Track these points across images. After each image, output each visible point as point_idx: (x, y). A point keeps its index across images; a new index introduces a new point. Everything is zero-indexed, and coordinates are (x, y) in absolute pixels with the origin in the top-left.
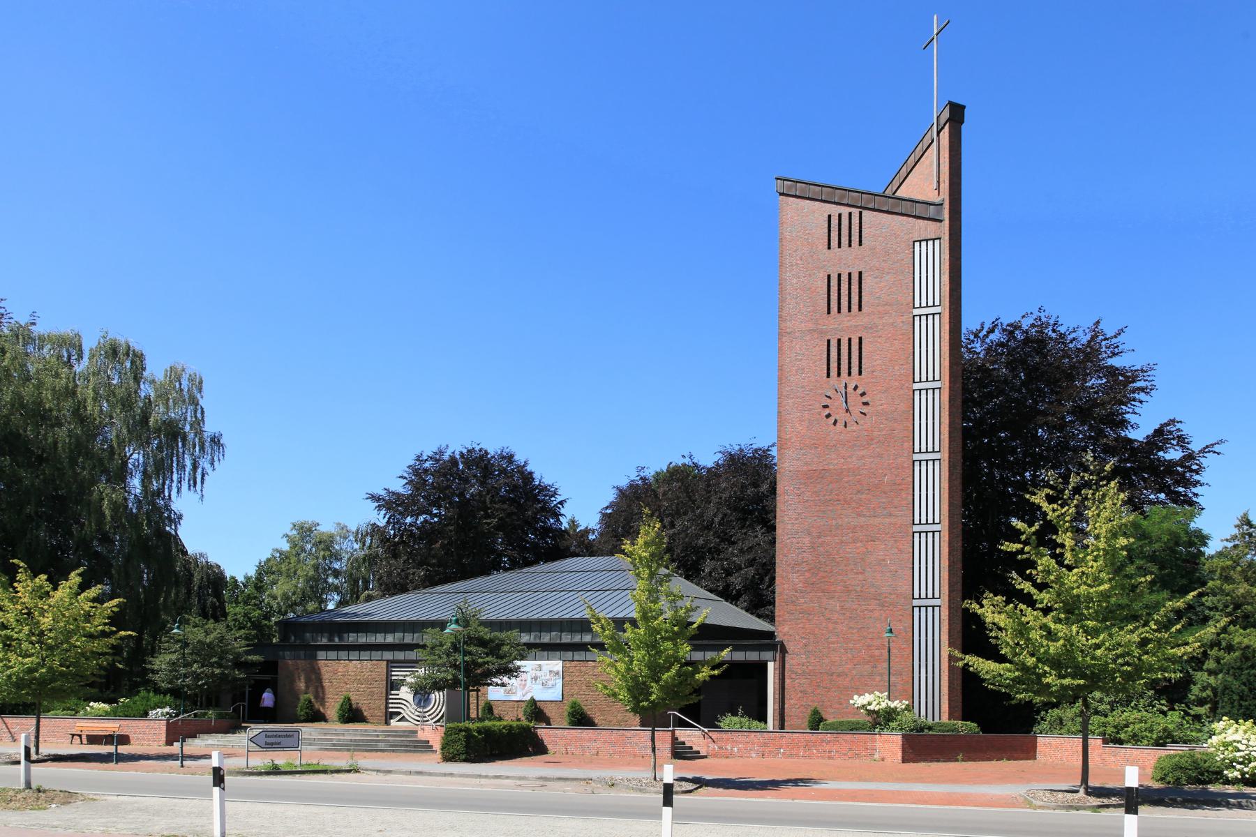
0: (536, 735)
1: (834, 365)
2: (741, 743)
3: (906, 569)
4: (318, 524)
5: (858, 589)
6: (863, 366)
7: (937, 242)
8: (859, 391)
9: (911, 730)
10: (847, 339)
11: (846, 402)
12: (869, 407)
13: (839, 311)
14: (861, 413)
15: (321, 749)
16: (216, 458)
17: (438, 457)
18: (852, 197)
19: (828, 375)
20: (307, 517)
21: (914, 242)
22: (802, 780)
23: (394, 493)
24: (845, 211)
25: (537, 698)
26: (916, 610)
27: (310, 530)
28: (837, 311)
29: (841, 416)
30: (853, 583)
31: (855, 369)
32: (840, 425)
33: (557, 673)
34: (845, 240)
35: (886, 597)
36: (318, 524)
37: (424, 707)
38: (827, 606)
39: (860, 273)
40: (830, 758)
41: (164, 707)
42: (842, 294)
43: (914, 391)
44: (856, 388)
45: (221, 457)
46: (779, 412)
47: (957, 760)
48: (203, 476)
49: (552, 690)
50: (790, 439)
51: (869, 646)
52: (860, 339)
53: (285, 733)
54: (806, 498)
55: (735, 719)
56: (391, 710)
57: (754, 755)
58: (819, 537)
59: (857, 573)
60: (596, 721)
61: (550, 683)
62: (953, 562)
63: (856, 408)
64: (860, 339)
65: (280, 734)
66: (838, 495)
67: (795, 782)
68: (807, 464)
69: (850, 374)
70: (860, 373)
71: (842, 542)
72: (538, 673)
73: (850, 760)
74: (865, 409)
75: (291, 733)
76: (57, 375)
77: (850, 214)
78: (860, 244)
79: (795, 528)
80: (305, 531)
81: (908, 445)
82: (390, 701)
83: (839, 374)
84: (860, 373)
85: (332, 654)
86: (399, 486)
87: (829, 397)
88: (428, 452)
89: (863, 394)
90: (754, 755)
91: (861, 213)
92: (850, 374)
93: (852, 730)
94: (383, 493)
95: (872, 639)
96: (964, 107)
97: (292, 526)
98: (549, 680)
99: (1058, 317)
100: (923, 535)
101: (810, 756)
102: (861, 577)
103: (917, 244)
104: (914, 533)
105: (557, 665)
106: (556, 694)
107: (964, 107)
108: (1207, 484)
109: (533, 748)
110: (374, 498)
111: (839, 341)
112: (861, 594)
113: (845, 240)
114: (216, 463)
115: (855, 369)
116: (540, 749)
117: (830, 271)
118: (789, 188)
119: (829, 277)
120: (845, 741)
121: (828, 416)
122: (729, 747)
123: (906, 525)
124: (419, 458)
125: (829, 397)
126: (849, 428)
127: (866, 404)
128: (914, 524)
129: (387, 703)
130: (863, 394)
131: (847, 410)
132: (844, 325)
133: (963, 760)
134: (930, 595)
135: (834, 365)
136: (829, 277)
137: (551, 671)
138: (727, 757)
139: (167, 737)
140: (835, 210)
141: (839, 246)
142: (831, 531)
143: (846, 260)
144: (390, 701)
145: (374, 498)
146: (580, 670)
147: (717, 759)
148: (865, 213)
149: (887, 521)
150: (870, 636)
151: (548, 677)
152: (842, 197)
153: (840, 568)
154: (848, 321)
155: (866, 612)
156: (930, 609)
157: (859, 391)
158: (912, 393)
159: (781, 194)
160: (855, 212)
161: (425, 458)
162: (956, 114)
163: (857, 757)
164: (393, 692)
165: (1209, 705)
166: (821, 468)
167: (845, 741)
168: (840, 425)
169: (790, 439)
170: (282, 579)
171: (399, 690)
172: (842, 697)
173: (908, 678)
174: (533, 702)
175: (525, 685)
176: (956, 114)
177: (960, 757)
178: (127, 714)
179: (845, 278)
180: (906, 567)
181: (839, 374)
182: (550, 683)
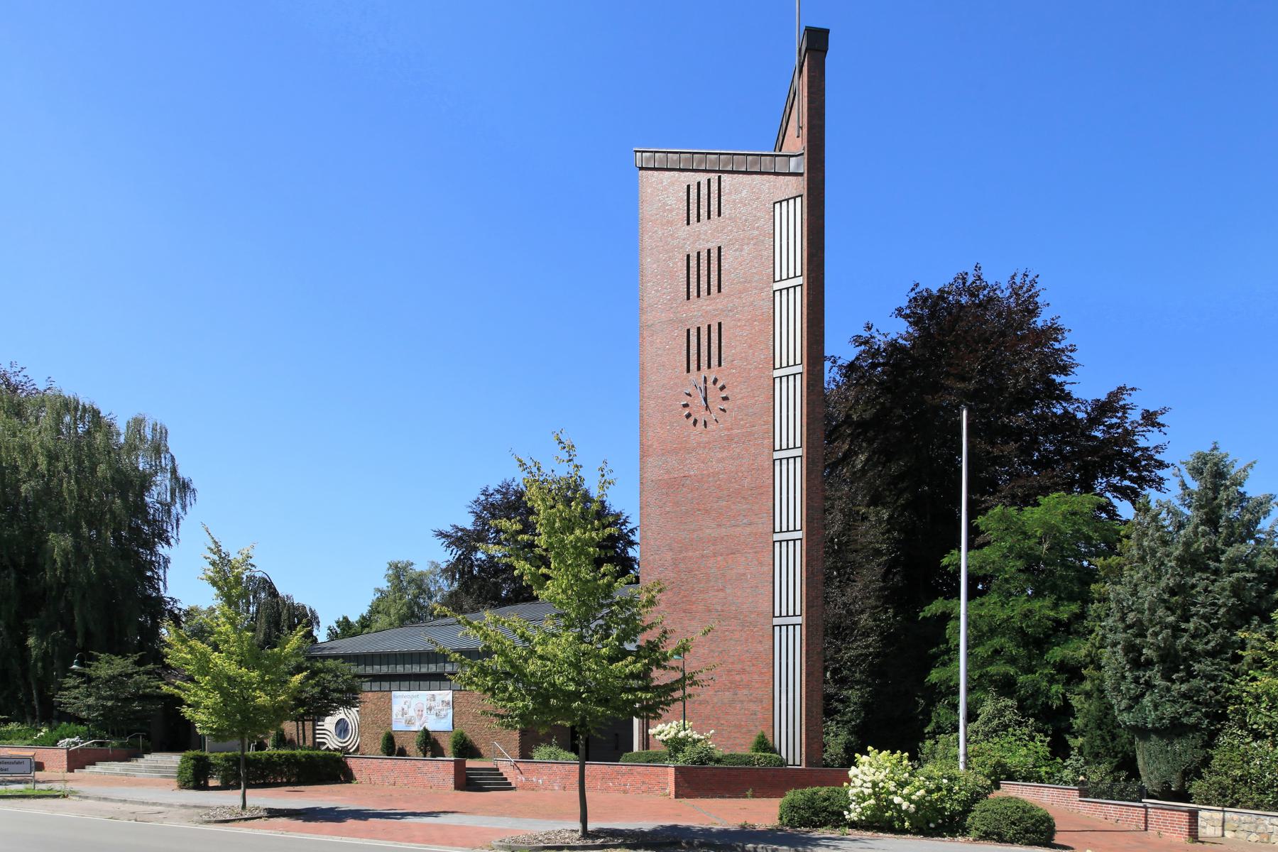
0: (346, 764)
1: (694, 357)
2: (545, 775)
3: (766, 584)
4: (412, 564)
5: (719, 608)
6: (723, 356)
7: (799, 200)
8: (719, 385)
9: (694, 763)
10: (706, 326)
11: (705, 399)
12: (729, 402)
13: (699, 296)
14: (721, 409)
15: (162, 777)
16: (188, 502)
17: (504, 490)
18: (710, 161)
19: (688, 371)
20: (401, 557)
21: (774, 204)
22: (434, 813)
23: (462, 530)
24: (703, 178)
25: (430, 728)
26: (777, 629)
27: (405, 569)
28: (696, 294)
29: (701, 415)
30: (714, 602)
31: (714, 361)
32: (700, 425)
33: (448, 703)
34: (704, 211)
35: (746, 616)
36: (412, 564)
37: (344, 738)
38: (689, 629)
39: (719, 248)
40: (625, 792)
41: (74, 737)
42: (701, 275)
43: (774, 379)
44: (715, 381)
45: (193, 502)
46: (641, 416)
47: (745, 797)
48: (178, 520)
49: (443, 721)
50: (651, 445)
51: (729, 671)
52: (720, 324)
53: (13, 760)
54: (667, 509)
55: (549, 749)
56: (318, 740)
57: (556, 788)
58: (681, 552)
59: (718, 591)
60: (482, 752)
61: (443, 713)
62: (812, 573)
63: (716, 404)
64: (720, 324)
65: (5, 760)
66: (698, 504)
67: (453, 812)
68: (668, 472)
69: (709, 366)
70: (720, 364)
71: (703, 556)
72: (433, 704)
73: (644, 795)
74: (725, 405)
75: (21, 760)
76: (14, 435)
77: (709, 181)
78: (719, 215)
79: (657, 543)
80: (399, 572)
81: (768, 442)
82: (318, 732)
83: (699, 368)
84: (720, 364)
85: (376, 686)
86: (468, 522)
87: (689, 395)
88: (493, 486)
89: (723, 388)
90: (556, 788)
91: (720, 177)
92: (709, 366)
93: (649, 762)
94: (449, 530)
95: (733, 663)
96: (827, 32)
97: (388, 566)
98: (441, 710)
99: (1038, 276)
100: (784, 544)
101: (607, 789)
102: (721, 594)
103: (777, 206)
104: (774, 542)
105: (447, 695)
106: (447, 724)
107: (827, 32)
108: (1172, 465)
109: (344, 777)
110: (441, 534)
111: (699, 329)
112: (722, 613)
113: (704, 211)
114: (188, 509)
115: (714, 361)
116: (348, 777)
117: (688, 249)
118: (648, 159)
119: (688, 256)
120: (639, 773)
121: (688, 416)
122: (534, 780)
123: (766, 534)
124: (484, 492)
125: (689, 395)
126: (710, 427)
127: (725, 399)
128: (774, 532)
129: (314, 734)
130: (723, 388)
131: (707, 407)
132: (702, 311)
133: (753, 796)
134: (791, 613)
135: (694, 357)
136: (688, 256)
137: (443, 701)
138: (533, 790)
139: (68, 764)
140: (692, 178)
141: (699, 220)
142: (692, 545)
143: (705, 235)
144: (318, 732)
145: (441, 534)
146: (467, 699)
147: (524, 791)
148: (724, 177)
149: (748, 530)
150: (730, 660)
151: (441, 707)
152: (700, 162)
153: (702, 585)
154: (707, 305)
155: (727, 633)
156: (791, 628)
157: (719, 385)
158: (772, 381)
159: (642, 168)
160: (714, 177)
161: (491, 492)
162: (817, 41)
163: (649, 791)
164: (319, 723)
165: (1137, 739)
166: (682, 475)
167: (639, 773)
168: (700, 425)
169: (651, 445)
170: (1210, 636)
171: (323, 721)
172: (704, 726)
173: (767, 702)
174: (426, 733)
175: (422, 715)
176: (817, 41)
177: (749, 793)
178: (43, 743)
179: (704, 255)
180: (767, 581)
181: (699, 368)
182: (443, 713)
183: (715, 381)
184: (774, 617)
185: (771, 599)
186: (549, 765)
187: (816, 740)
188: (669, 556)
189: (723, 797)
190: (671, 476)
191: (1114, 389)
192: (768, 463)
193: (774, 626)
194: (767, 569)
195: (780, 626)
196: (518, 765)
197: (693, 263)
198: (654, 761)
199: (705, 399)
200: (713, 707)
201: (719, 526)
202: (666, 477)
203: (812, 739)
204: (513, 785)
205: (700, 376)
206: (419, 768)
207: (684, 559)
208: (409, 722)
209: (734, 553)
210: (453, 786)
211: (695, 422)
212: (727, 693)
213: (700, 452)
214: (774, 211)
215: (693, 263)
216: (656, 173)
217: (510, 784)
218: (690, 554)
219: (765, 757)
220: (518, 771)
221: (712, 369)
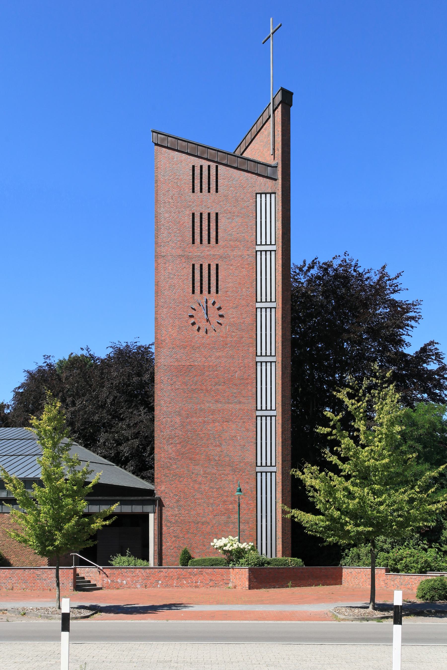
1: (197, 284)
5: (217, 458)
8: (217, 306)
11: (207, 314)
19: (193, 292)
21: (256, 194)
24: (205, 164)
29: (203, 325)
31: (213, 289)
32: (202, 332)
35: (237, 465)
40: (196, 587)
44: (214, 303)
46: (156, 319)
47: (287, 587)
51: (224, 502)
52: (217, 265)
55: (124, 558)
57: (139, 586)
58: (187, 417)
59: (216, 446)
60: (12, 562)
62: (285, 439)
63: (214, 319)
64: (217, 265)
67: (169, 607)
68: (177, 360)
69: (209, 292)
71: (204, 422)
73: (211, 588)
74: (221, 320)
81: (252, 349)
83: (201, 292)
89: (219, 309)
90: (139, 586)
92: (209, 292)
93: (212, 565)
101: (182, 586)
102: (218, 449)
104: (257, 416)
113: (205, 186)
115: (213, 289)
117: (194, 209)
120: (208, 574)
122: (119, 581)
123: (251, 410)
130: (219, 309)
133: (292, 586)
135: (197, 284)
140: (198, 162)
141: (201, 192)
149: (238, 407)
152: (203, 152)
153: (203, 442)
157: (217, 306)
158: (255, 310)
159: (157, 144)
160: (213, 165)
166: (188, 364)
167: (208, 574)
168: (202, 332)
177: (290, 584)
179: (205, 216)
180: (252, 442)
183: (214, 303)
184: (257, 466)
185: (255, 454)
186: (132, 570)
187: (287, 548)
188: (178, 420)
189: (310, 585)
190: (180, 363)
191: (422, 346)
192: (252, 364)
193: (257, 472)
194: (253, 434)
195: (261, 472)
196: (105, 570)
197: (197, 220)
198: (216, 565)
199: (207, 314)
200: (213, 527)
201: (217, 401)
202: (176, 364)
203: (285, 548)
204: (98, 586)
205: (202, 298)
206: (38, 575)
207: (190, 423)
208: (164, 537)
209: (228, 422)
210: (72, 588)
211: (199, 329)
212: (223, 517)
213: (203, 350)
214: (256, 198)
215: (197, 220)
216: (168, 150)
217: (95, 585)
218: (195, 419)
219: (294, 560)
220: (104, 575)
221: (211, 295)
